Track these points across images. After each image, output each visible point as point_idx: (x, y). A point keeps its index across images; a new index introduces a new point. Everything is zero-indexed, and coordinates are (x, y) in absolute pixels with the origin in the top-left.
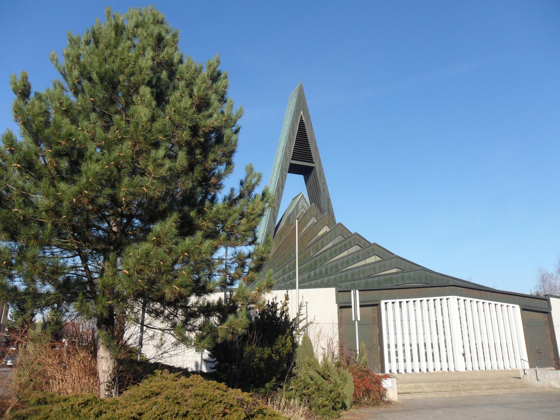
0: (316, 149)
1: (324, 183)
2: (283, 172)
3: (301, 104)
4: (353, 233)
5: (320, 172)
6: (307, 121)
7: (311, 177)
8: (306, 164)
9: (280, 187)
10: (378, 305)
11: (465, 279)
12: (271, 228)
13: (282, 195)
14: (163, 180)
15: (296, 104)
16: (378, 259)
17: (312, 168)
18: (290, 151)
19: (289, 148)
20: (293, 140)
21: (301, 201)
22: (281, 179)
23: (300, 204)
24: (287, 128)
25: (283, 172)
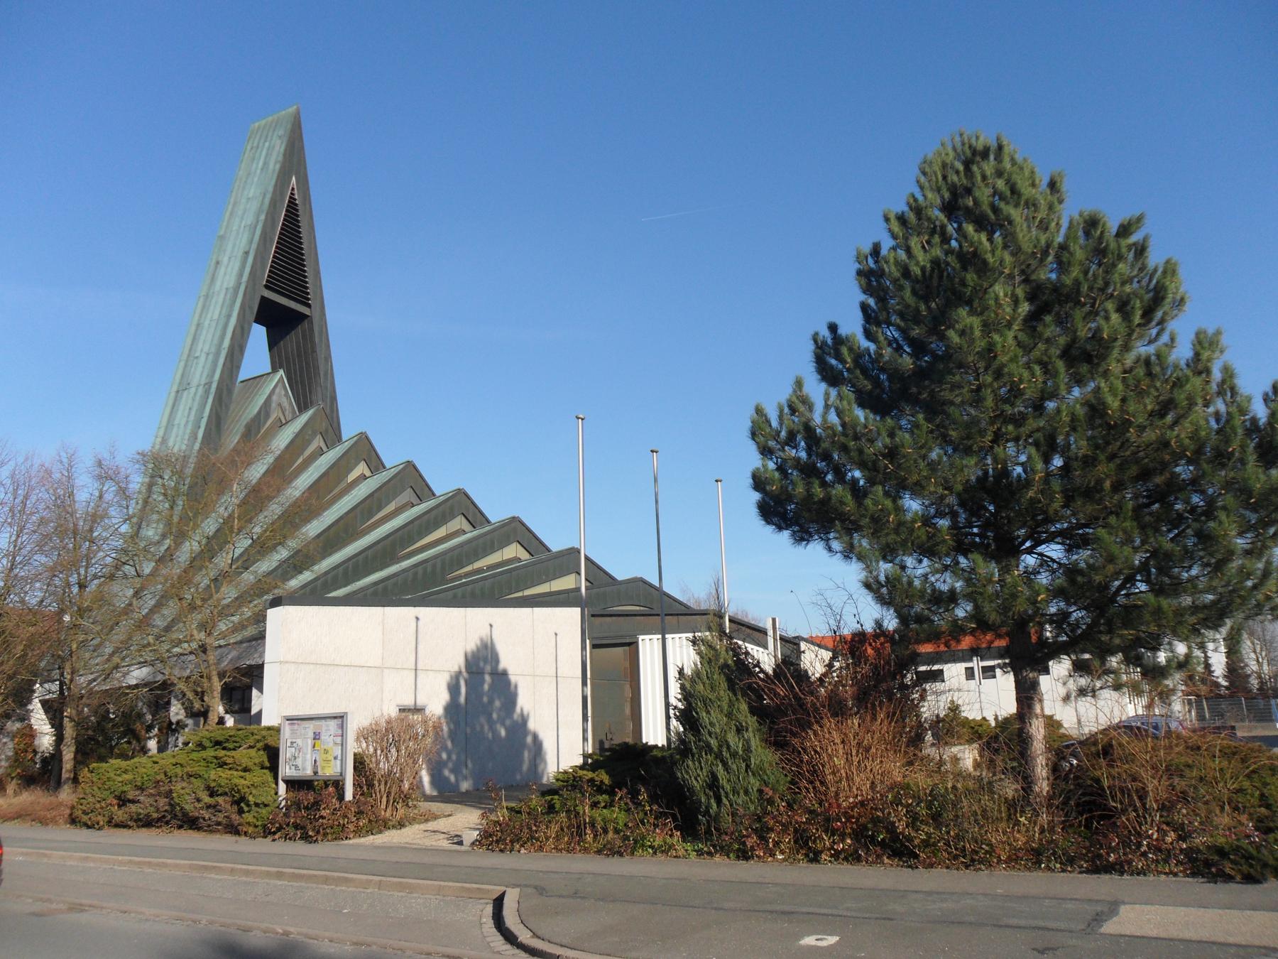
0: (317, 273)
1: (328, 358)
3: (294, 160)
5: (321, 332)
7: (292, 341)
9: (237, 348)
10: (633, 646)
11: (469, 610)
14: (972, 391)
15: (284, 155)
17: (302, 317)
21: (277, 390)
23: (274, 398)
24: (254, 206)
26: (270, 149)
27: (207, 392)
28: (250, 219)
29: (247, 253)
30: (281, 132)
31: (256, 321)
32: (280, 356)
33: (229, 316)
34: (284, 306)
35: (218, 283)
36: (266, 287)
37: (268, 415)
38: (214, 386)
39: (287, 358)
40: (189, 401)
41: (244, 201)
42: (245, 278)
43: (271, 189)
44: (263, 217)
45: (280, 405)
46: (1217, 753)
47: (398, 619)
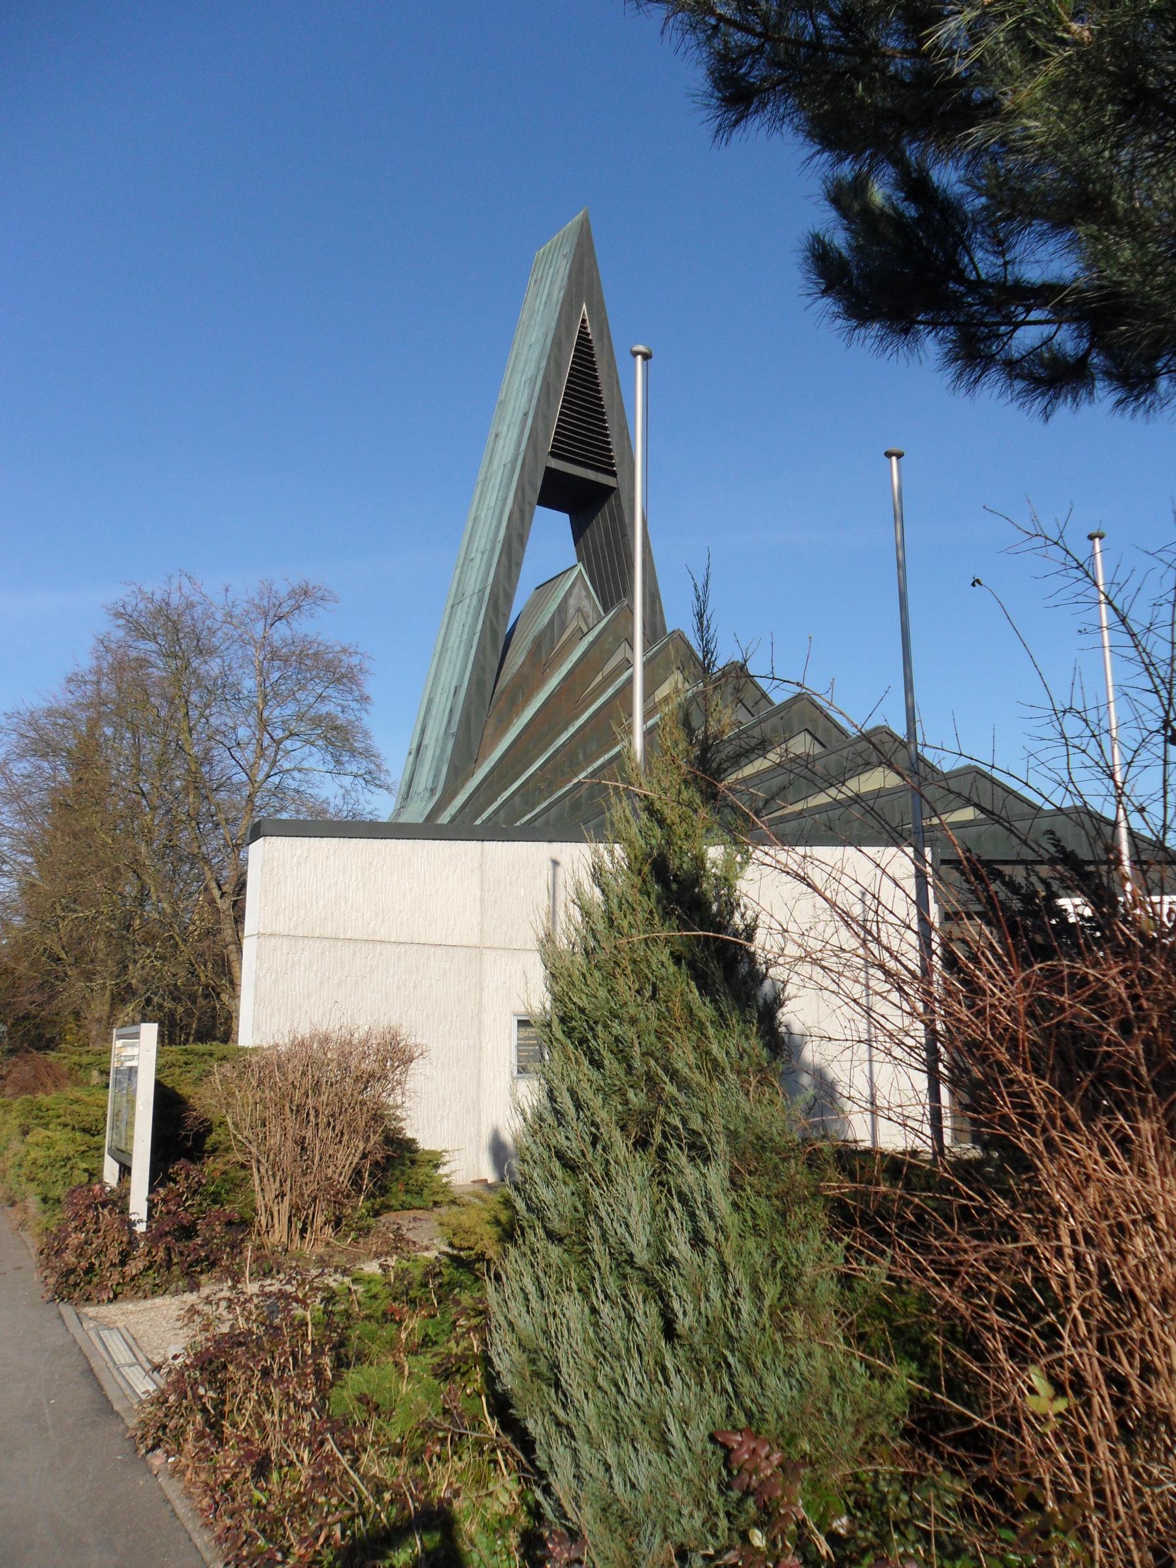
2: (523, 490)
3: (583, 281)
4: (779, 696)
6: (601, 338)
7: (600, 523)
8: (591, 475)
12: (483, 668)
13: (519, 565)
15: (569, 277)
16: (893, 780)
17: (607, 492)
18: (547, 426)
19: (545, 417)
20: (558, 392)
21: (576, 591)
22: (517, 515)
24: (535, 353)
25: (523, 490)
26: (555, 274)
27: (480, 601)
28: (530, 370)
29: (526, 415)
30: (566, 250)
31: (542, 502)
32: (587, 547)
33: (505, 499)
34: (579, 477)
35: (496, 461)
36: (552, 454)
37: (563, 627)
38: (488, 591)
39: (595, 550)
40: (463, 616)
41: (526, 349)
42: (523, 447)
43: (553, 325)
44: (544, 364)
45: (579, 610)
46: (396, 1305)
47: (538, 852)
